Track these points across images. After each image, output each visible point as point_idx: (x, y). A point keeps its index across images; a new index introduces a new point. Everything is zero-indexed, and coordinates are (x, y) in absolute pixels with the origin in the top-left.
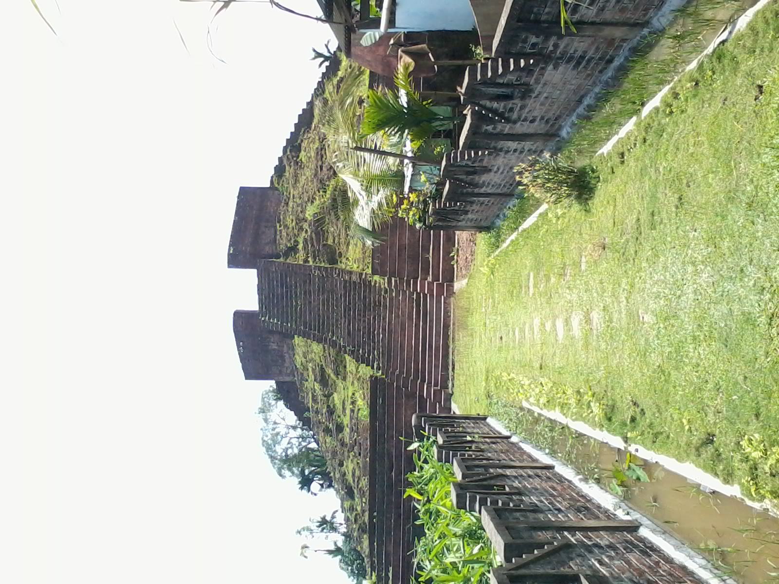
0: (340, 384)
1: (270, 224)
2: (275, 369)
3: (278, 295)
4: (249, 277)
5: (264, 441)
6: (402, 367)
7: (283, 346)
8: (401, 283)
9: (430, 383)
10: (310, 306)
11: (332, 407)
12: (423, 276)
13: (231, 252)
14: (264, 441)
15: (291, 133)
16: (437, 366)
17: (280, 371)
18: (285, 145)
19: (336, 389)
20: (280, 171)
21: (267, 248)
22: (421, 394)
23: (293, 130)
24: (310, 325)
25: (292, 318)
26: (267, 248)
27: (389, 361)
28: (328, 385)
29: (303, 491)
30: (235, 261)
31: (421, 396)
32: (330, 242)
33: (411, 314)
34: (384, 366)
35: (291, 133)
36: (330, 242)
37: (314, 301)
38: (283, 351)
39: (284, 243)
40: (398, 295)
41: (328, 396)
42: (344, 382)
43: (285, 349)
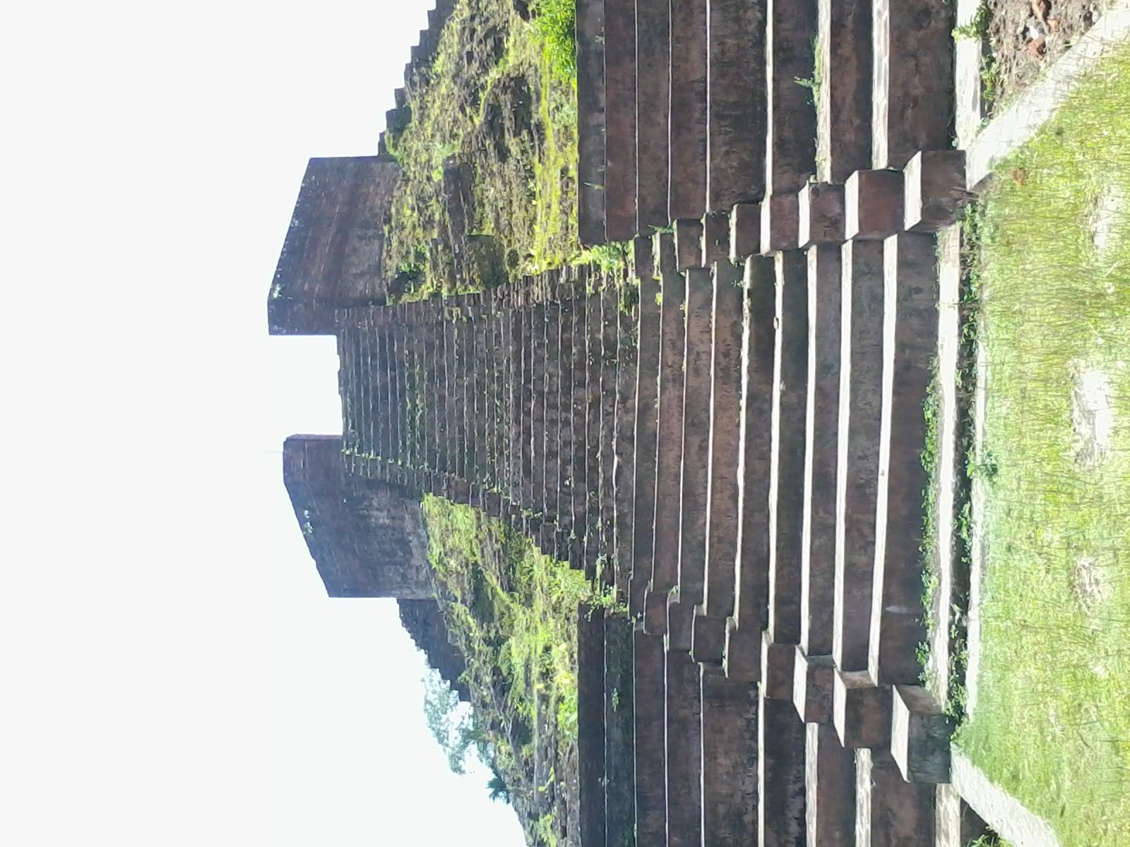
0: (520, 615)
1: (370, 233)
2: (391, 574)
3: (375, 389)
4: (320, 355)
5: (427, 702)
6: (692, 577)
7: (403, 519)
8: (690, 242)
9: (820, 648)
10: (442, 409)
11: (505, 673)
12: (786, 180)
13: (276, 295)
14: (427, 702)
15: (422, 32)
16: (859, 577)
17: (404, 576)
18: (409, 61)
19: (512, 626)
20: (398, 120)
21: (360, 285)
22: (781, 694)
23: (426, 27)
24: (443, 461)
25: (404, 443)
26: (360, 285)
27: (642, 551)
28: (492, 615)
29: (497, 799)
30: (288, 314)
31: (780, 704)
32: (488, 229)
33: (728, 374)
34: (624, 571)
35: (422, 32)
36: (488, 229)
37: (451, 394)
38: (402, 530)
39: (394, 265)
40: (675, 294)
41: (496, 643)
42: (528, 612)
43: (408, 525)
